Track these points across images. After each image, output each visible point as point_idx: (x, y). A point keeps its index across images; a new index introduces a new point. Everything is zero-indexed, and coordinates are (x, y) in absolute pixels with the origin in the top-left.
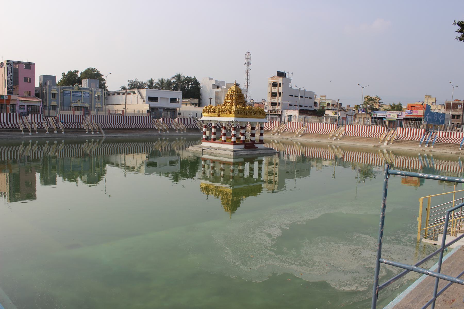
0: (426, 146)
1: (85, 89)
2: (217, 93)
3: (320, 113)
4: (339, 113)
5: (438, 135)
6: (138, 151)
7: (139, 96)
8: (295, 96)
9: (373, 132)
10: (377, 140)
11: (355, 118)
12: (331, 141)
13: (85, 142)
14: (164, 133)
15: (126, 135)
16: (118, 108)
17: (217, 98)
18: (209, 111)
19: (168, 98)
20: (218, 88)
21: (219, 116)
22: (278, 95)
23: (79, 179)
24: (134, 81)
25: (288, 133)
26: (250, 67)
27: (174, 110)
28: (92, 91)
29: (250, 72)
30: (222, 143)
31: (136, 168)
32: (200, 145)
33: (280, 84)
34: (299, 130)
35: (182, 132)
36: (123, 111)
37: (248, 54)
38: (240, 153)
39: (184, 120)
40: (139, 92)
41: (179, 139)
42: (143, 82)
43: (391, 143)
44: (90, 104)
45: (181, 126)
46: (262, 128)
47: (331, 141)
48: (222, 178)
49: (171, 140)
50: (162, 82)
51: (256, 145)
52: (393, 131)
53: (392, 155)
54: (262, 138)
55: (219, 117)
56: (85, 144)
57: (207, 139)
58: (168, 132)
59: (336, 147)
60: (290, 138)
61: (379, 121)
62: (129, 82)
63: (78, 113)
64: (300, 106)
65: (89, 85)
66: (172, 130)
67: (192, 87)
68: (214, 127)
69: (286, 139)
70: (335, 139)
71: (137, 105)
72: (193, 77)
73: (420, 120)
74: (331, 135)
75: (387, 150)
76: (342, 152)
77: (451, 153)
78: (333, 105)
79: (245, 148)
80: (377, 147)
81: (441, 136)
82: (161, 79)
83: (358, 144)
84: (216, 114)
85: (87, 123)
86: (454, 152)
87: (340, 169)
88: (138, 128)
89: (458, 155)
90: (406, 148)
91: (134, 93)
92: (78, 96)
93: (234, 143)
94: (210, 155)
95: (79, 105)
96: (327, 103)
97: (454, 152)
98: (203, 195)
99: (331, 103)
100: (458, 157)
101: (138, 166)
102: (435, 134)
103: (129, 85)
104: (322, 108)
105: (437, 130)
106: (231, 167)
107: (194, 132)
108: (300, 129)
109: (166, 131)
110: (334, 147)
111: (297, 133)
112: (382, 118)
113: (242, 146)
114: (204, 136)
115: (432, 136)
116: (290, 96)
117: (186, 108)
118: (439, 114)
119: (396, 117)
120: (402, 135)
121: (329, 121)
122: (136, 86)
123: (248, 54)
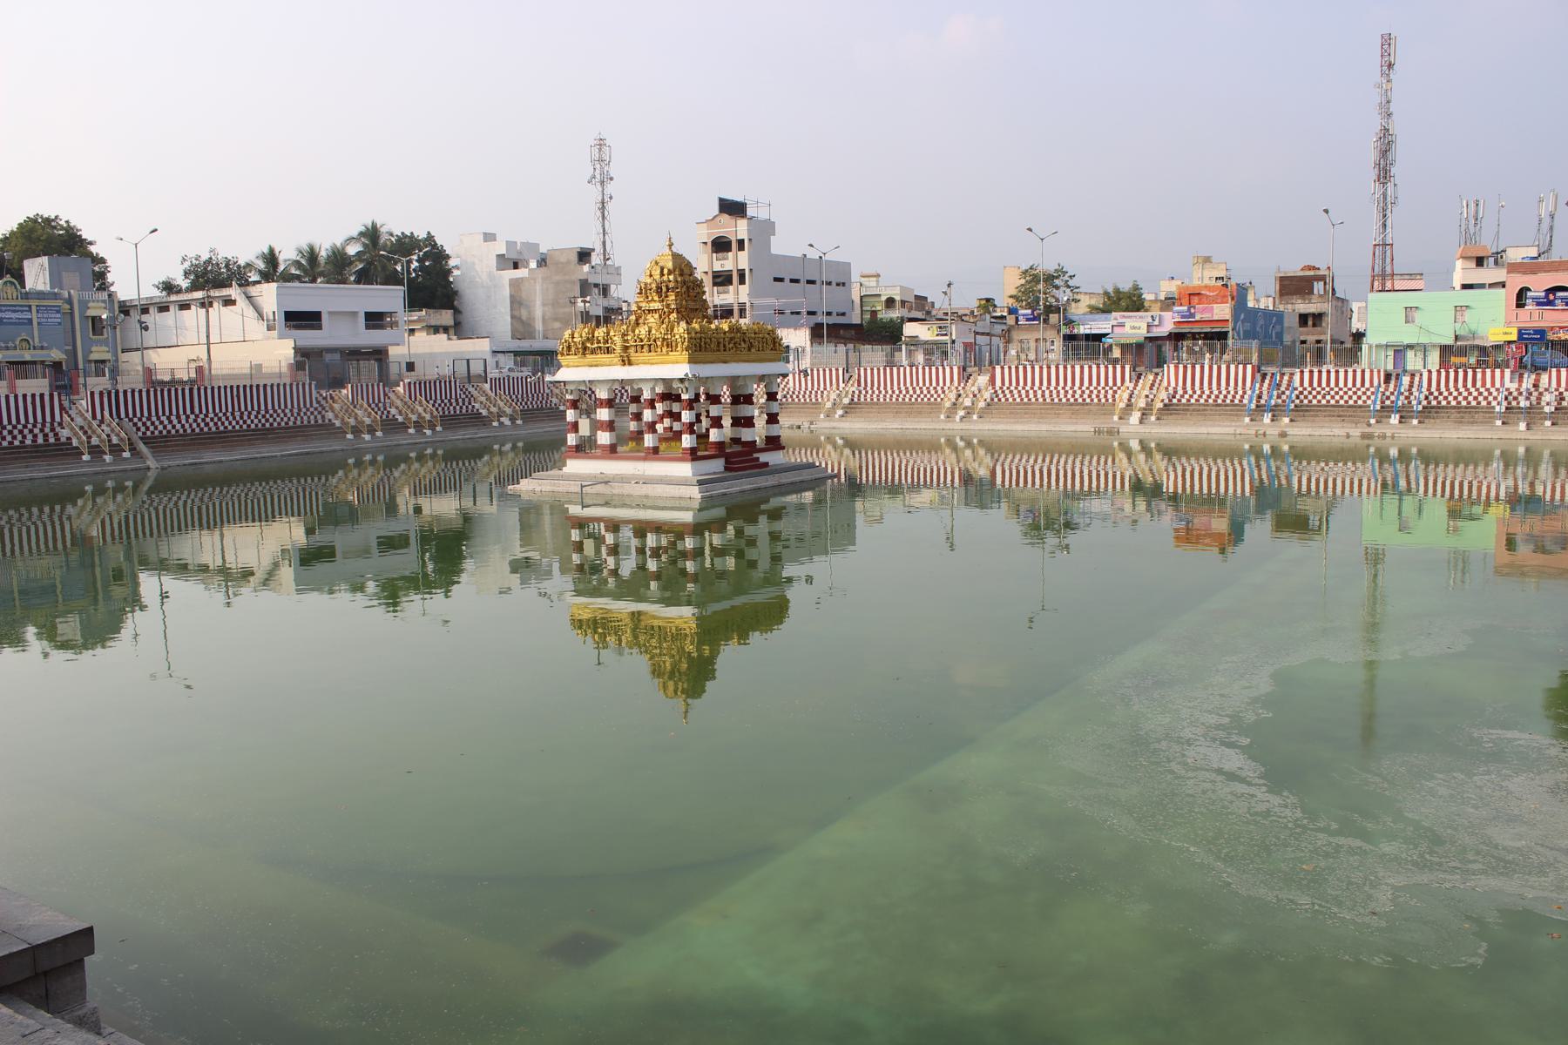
0: (1267, 418)
1: (41, 295)
2: (515, 284)
3: (883, 333)
5: (1297, 382)
6: (264, 515)
7: (250, 312)
8: (792, 281)
9: (1086, 383)
10: (1106, 408)
11: (1008, 341)
12: (949, 426)
13: (82, 494)
14: (367, 437)
15: (216, 456)
16: (172, 362)
17: (516, 302)
18: (585, 348)
19: (354, 314)
20: (516, 266)
21: (626, 361)
22: (735, 278)
23: (31, 631)
24: (205, 257)
25: (822, 404)
26: (610, 188)
27: (379, 354)
28: (70, 301)
29: (609, 207)
30: (645, 459)
31: (260, 575)
32: (554, 472)
33: (741, 243)
34: (833, 396)
35: (428, 432)
36: (199, 370)
37: (601, 143)
38: (719, 489)
39: (426, 388)
40: (249, 298)
41: (421, 458)
42: (242, 262)
43: (1153, 418)
44: (66, 352)
45: (420, 409)
46: (772, 396)
47: (949, 426)
48: (653, 585)
49: (393, 461)
50: (312, 256)
51: (764, 457)
52: (1151, 377)
53: (1158, 457)
54: (774, 430)
56: (80, 502)
57: (584, 449)
58: (379, 434)
59: (969, 444)
60: (806, 425)
61: (1088, 346)
62: (187, 265)
63: (37, 385)
64: (809, 313)
65: (55, 279)
66: (391, 426)
67: (422, 268)
69: (791, 427)
71: (245, 343)
72: (422, 235)
73: (1223, 336)
74: (948, 404)
75: (1141, 442)
76: (988, 460)
77: (1348, 436)
78: (903, 303)
79: (726, 469)
80: (1110, 432)
81: (1306, 384)
82: (266, 251)
83: (1044, 427)
84: (614, 358)
85: (79, 421)
86: (1356, 432)
87: (968, 517)
88: (272, 429)
89: (1366, 442)
90: (1204, 430)
91: (229, 302)
92: (20, 323)
93: (693, 455)
94: (607, 504)
95: (28, 358)
96: (884, 298)
97: (1356, 432)
98: (585, 646)
99: (898, 298)
100: (1368, 446)
101: (266, 562)
102: (1286, 378)
103: (186, 274)
104: (867, 316)
105: (1293, 366)
106: (689, 543)
107: (542, 426)
108: (834, 393)
109: (371, 430)
110: (961, 444)
111: (829, 405)
112: (1098, 338)
113: (718, 465)
114: (571, 439)
115: (1279, 385)
116: (776, 279)
117: (423, 346)
118: (1265, 312)
119: (1143, 332)
120: (1184, 388)
121: (920, 358)
122: (212, 279)
123: (601, 143)
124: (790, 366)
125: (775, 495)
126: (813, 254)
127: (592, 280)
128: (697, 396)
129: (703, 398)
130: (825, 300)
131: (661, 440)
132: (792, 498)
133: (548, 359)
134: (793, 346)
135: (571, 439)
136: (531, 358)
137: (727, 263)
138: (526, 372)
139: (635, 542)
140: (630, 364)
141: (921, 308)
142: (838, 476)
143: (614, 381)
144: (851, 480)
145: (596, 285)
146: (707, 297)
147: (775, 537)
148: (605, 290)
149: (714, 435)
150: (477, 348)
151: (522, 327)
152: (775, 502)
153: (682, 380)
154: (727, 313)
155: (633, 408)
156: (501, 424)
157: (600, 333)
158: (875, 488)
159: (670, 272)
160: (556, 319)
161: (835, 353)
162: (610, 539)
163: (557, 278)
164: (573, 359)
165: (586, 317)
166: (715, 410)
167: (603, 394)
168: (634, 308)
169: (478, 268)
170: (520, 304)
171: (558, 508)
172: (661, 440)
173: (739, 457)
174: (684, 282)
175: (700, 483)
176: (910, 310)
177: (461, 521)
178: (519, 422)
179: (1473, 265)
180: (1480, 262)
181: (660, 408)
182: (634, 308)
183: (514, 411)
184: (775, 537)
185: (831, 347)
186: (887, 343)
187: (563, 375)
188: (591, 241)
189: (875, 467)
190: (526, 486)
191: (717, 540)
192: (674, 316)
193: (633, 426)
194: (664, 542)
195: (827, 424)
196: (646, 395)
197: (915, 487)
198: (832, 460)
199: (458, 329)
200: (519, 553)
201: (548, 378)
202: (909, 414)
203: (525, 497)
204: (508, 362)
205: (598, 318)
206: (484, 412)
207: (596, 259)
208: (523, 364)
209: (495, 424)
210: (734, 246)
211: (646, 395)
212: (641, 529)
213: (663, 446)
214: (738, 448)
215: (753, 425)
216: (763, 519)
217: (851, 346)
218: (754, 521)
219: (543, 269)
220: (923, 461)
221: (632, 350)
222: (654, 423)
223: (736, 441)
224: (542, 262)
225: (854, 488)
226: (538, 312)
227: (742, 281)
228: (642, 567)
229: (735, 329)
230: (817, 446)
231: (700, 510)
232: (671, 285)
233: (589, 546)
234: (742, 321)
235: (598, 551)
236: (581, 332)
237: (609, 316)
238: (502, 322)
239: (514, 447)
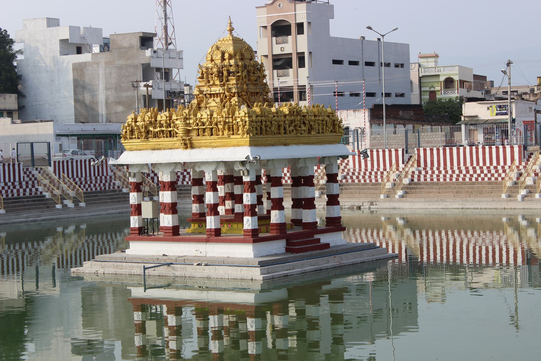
2: (79, 69)
3: (445, 115)
4: (513, 106)
8: (351, 63)
12: (511, 205)
17: (80, 86)
18: (148, 132)
20: (79, 51)
21: (189, 145)
25: (381, 187)
30: (207, 241)
34: (393, 176)
38: (281, 271)
45: (65, 187)
46: (332, 178)
47: (511, 205)
51: (324, 239)
54: (335, 211)
55: (189, 151)
57: (146, 231)
60: (367, 205)
68: (172, 186)
69: (351, 208)
70: (524, 197)
74: (509, 184)
78: (462, 83)
79: (288, 250)
84: (176, 141)
93: (255, 237)
94: (168, 286)
96: (442, 79)
99: (456, 78)
104: (426, 97)
107: (105, 209)
110: (524, 223)
111: (388, 185)
113: (279, 246)
114: (134, 222)
116: (335, 62)
121: (480, 137)
124: (350, 148)
125: (337, 276)
126: (371, 37)
127: (155, 64)
128: (259, 178)
129: (264, 180)
130: (384, 81)
131: (223, 221)
132: (352, 279)
133: (111, 142)
134: (352, 128)
135: (134, 222)
136: (94, 141)
137: (288, 46)
138: (89, 155)
139: (196, 324)
140: (192, 147)
141: (480, 87)
142: (399, 256)
143: (176, 164)
144: (411, 259)
145: (158, 70)
146: (267, 80)
147: (337, 319)
148: (167, 75)
149: (275, 217)
150: (41, 131)
151: (85, 111)
152: (336, 283)
153: (243, 163)
154: (286, 95)
155: (195, 191)
156: (65, 206)
157: (162, 116)
158: (436, 267)
159: (231, 57)
160: (119, 103)
161: (395, 134)
162: (172, 320)
163: (121, 62)
164: (136, 142)
165: (148, 101)
166: (275, 193)
167: (165, 177)
168: (196, 92)
169: (41, 52)
170: (84, 88)
171: (121, 291)
172: (223, 221)
173: (300, 239)
174: (245, 67)
175: (262, 264)
176: (469, 89)
177: (22, 304)
178: (82, 204)
181: (222, 190)
182: (196, 92)
183: (78, 193)
184: (337, 319)
185: (391, 128)
186: (446, 123)
187: (126, 158)
188: (152, 25)
189: (436, 246)
190: (89, 269)
191: (278, 321)
192: (235, 99)
193: (195, 208)
194: (226, 324)
195: (387, 205)
196: (208, 178)
197: (478, 268)
198: (394, 242)
199: (22, 113)
200: (81, 333)
201: (111, 161)
203: (88, 279)
204: (71, 145)
205: (160, 101)
206: (48, 195)
207: (158, 44)
208: (87, 147)
209: (59, 206)
210: (294, 29)
211: (208, 178)
212: (203, 311)
213: (225, 228)
214: (298, 230)
215: (314, 207)
216: (324, 300)
217: (410, 127)
218: (315, 301)
219: (106, 54)
220: (486, 239)
221: (194, 134)
222: (216, 206)
223: (297, 222)
224: (105, 47)
225: (416, 267)
226: (101, 97)
227: (301, 64)
228: (204, 349)
229: (295, 112)
230: (377, 226)
231: (262, 291)
232: (232, 69)
233: (151, 326)
234: (302, 104)
235: (160, 333)
236: (144, 116)
237: (170, 100)
238: (64, 106)
239: (77, 230)
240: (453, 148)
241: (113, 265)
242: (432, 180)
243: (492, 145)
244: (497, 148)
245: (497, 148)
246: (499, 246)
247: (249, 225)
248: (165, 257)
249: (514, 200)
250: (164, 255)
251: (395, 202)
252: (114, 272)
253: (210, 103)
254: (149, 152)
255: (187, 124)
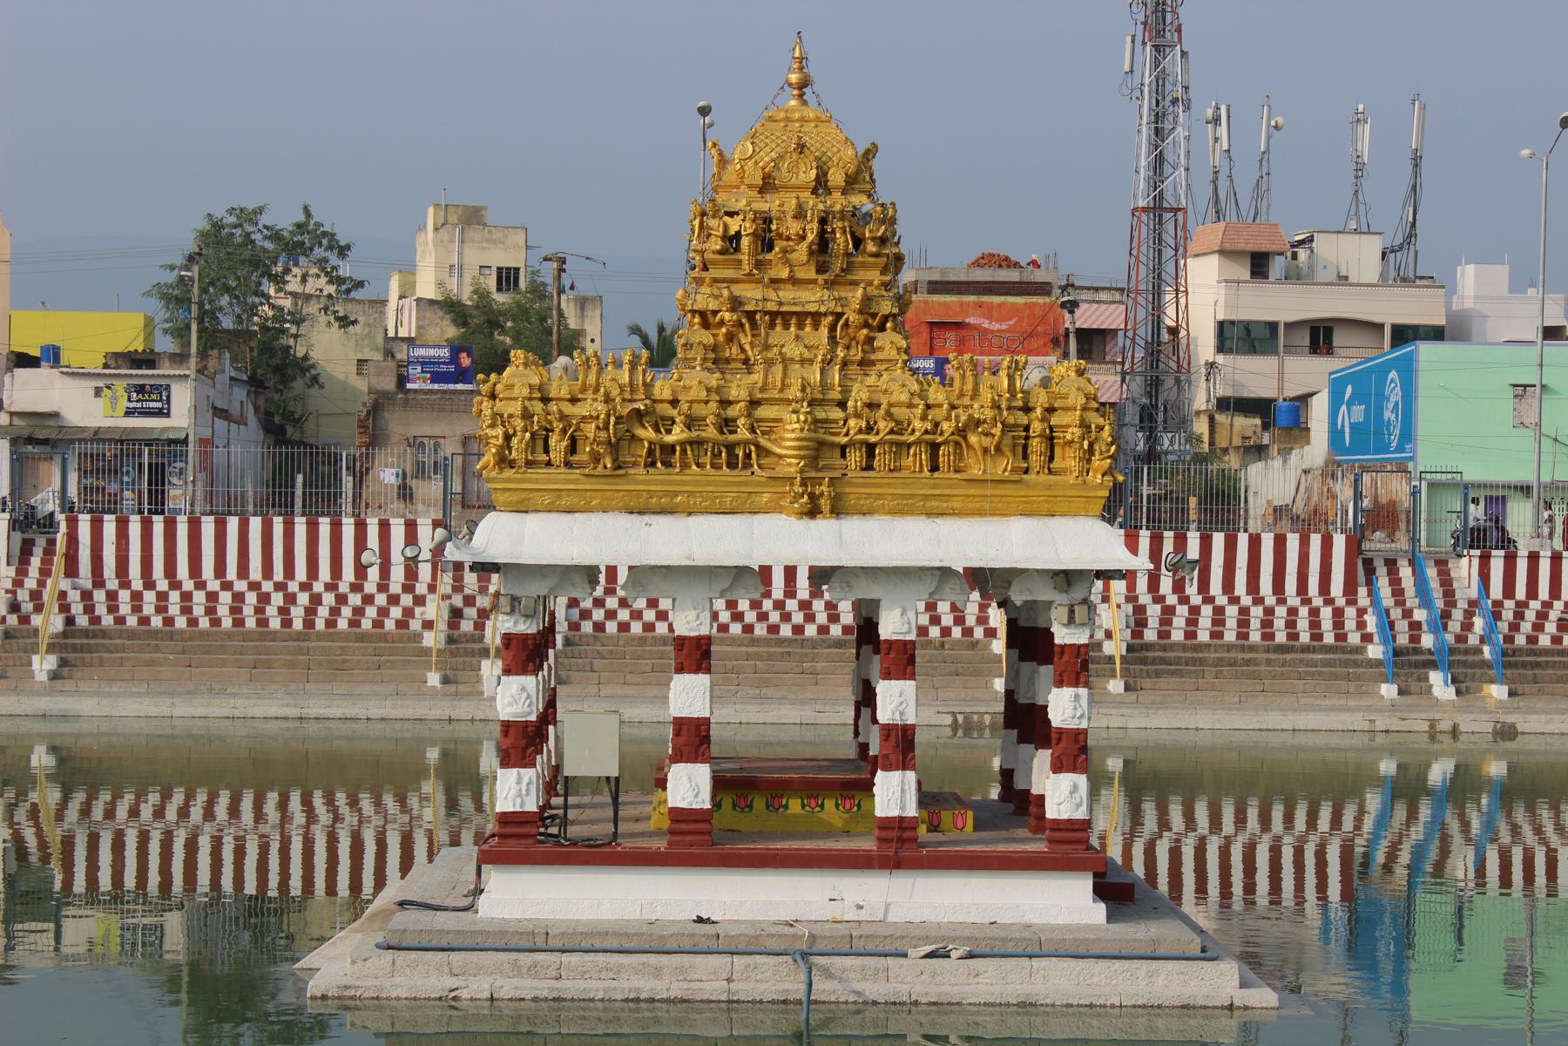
9: (325, 573)
140: (837, 511)
179: (1246, 274)
180: (1259, 264)
202: (338, 669)
240: (106, 517)
241: (516, 965)
242: (262, 622)
243: (103, 512)
244: (122, 524)
245: (122, 524)
246: (282, 836)
247: (1079, 805)
248: (707, 928)
249: (469, 694)
250: (700, 920)
251: (32, 693)
252: (545, 993)
253: (881, 349)
254: (624, 520)
255: (816, 421)
